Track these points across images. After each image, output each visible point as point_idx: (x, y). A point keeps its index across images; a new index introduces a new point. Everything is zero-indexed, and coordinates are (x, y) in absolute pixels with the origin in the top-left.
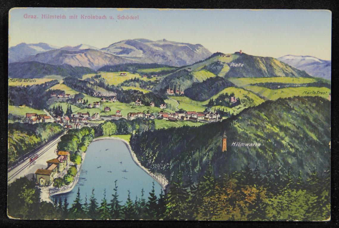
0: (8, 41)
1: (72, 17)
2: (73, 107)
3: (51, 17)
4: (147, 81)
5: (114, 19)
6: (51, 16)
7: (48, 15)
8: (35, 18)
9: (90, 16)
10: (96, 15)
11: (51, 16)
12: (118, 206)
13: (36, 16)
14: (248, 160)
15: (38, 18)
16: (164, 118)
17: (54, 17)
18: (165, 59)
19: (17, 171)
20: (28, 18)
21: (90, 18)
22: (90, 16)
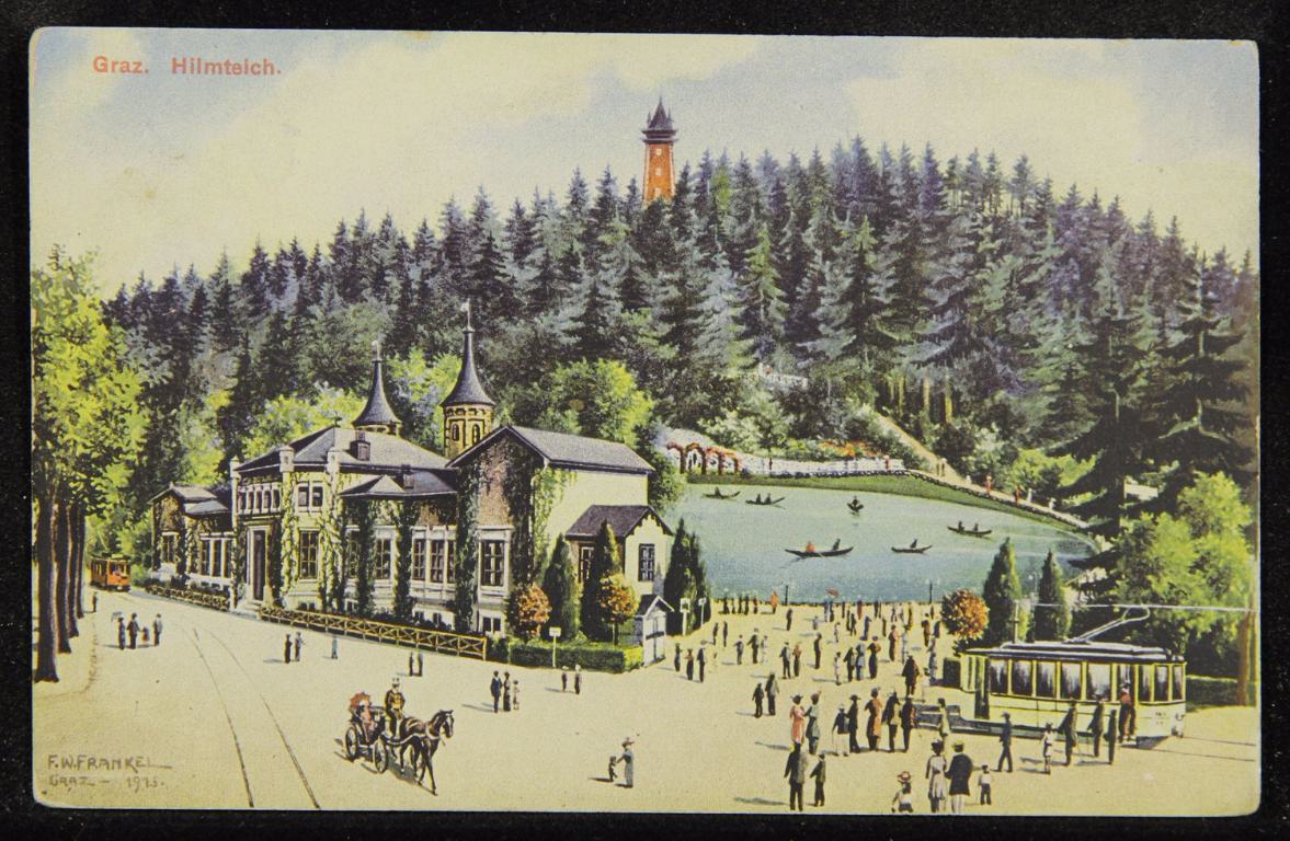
0: (1261, 222)
1: (217, 68)
2: (369, 289)
3: (210, 67)
4: (1232, 263)
5: (279, 72)
6: (207, 65)
7: (196, 62)
8: (136, 71)
9: (91, 67)
10: (265, 61)
11: (207, 65)
12: (344, 388)
13: (139, 64)
14: (904, 323)
15: (147, 71)
16: (823, 301)
17: (224, 67)
18: (798, 172)
19: (1111, 672)
20: (243, 75)
21: (252, 68)
22: (242, 63)
